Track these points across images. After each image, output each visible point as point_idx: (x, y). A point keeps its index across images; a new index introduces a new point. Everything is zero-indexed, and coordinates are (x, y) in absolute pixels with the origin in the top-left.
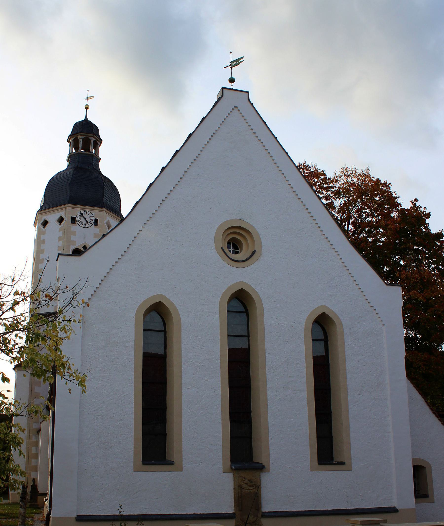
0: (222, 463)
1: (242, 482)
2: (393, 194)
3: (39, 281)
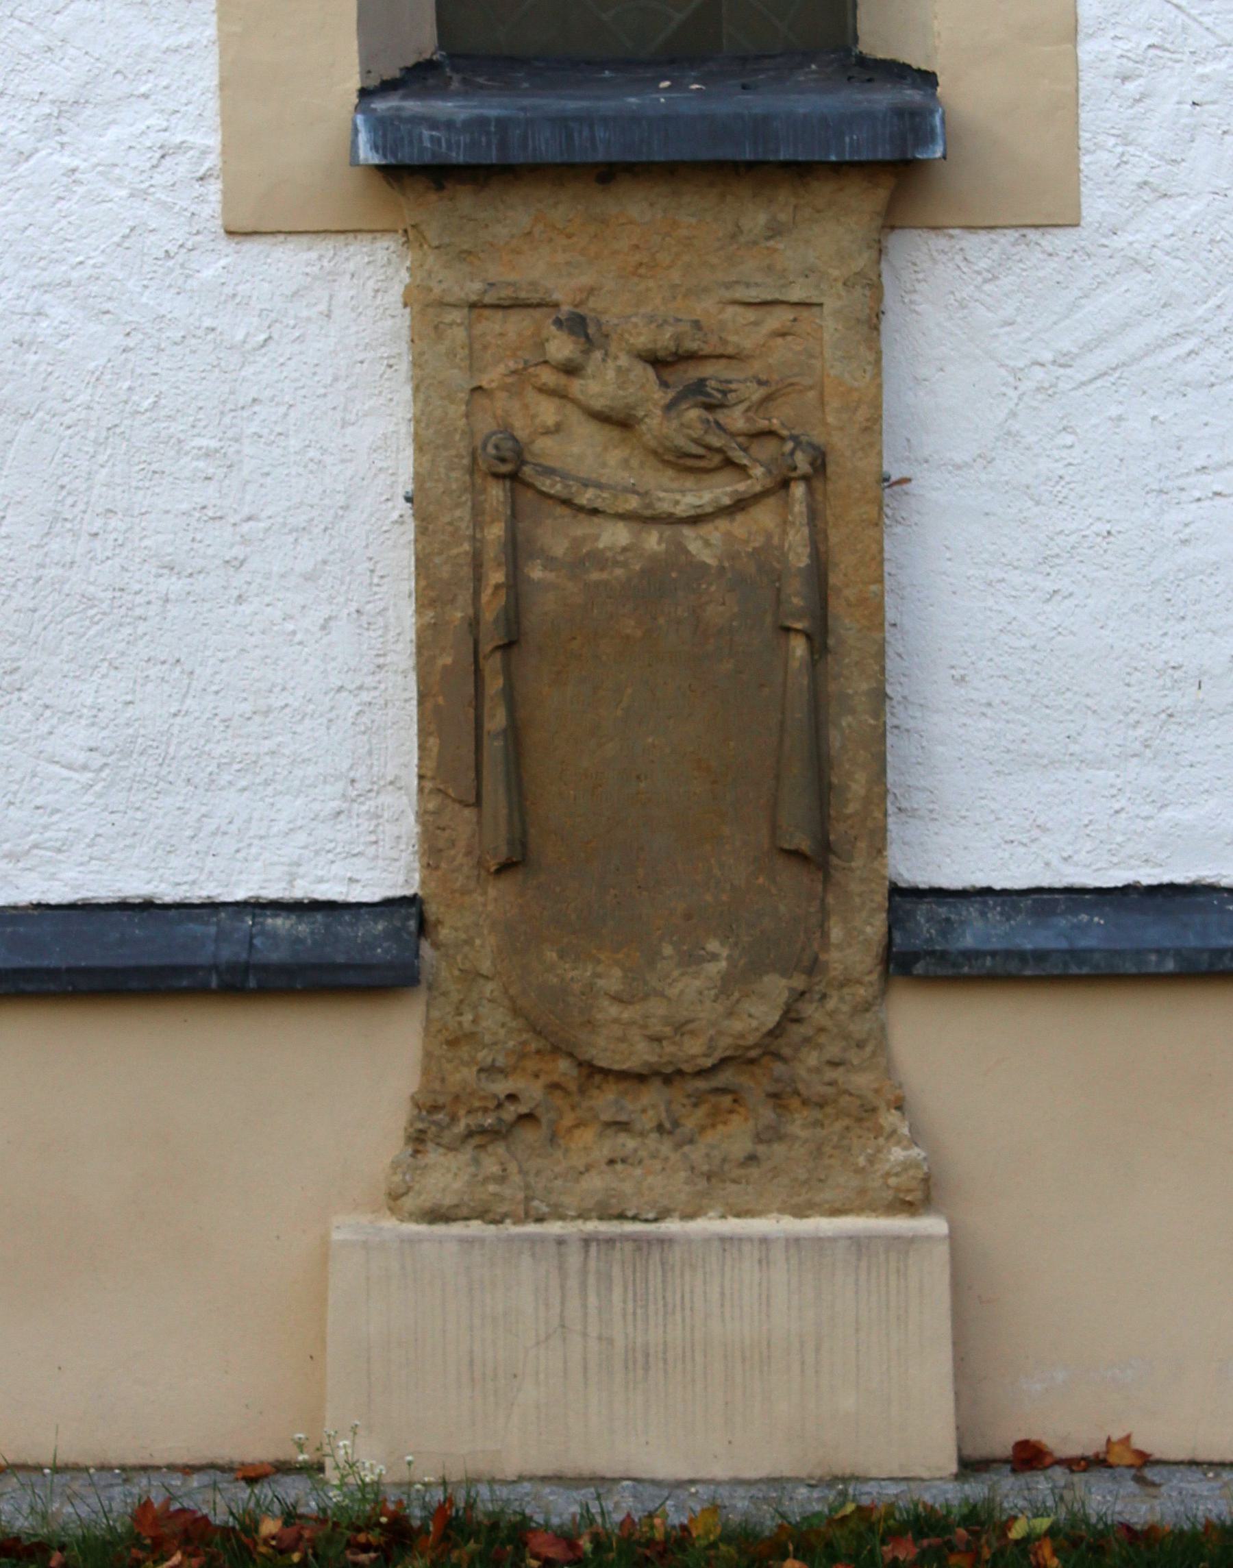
1: (543, 390)
3: (1018, 223)
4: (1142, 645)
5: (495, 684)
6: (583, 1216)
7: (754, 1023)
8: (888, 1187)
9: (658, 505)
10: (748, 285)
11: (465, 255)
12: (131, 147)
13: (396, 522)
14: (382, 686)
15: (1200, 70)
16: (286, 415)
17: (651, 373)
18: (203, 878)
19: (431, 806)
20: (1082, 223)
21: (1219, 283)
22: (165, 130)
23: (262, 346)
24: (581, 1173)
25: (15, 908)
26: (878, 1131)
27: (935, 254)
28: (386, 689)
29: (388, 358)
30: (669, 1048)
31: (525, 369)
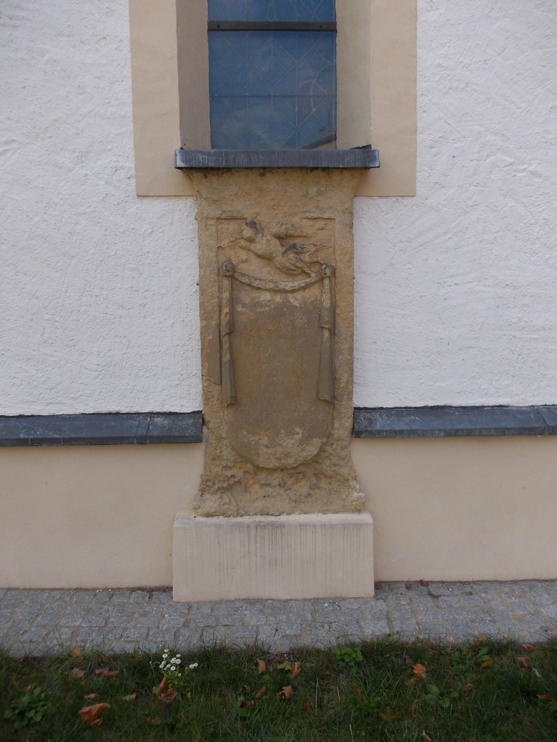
0: (130, 142)
1: (242, 248)
2: (284, 690)
4: (431, 332)
5: (226, 346)
6: (256, 514)
7: (310, 453)
8: (353, 505)
9: (280, 286)
10: (310, 212)
11: (215, 202)
12: (105, 167)
13: (195, 292)
14: (191, 345)
15: (455, 145)
16: (158, 257)
17: (278, 242)
18: (135, 405)
19: (205, 385)
20: (417, 195)
21: (459, 216)
22: (116, 161)
23: (150, 234)
24: (255, 501)
25: (75, 414)
26: (349, 487)
27: (369, 205)
28: (192, 345)
29: (191, 238)
30: (283, 461)
31: (235, 240)
